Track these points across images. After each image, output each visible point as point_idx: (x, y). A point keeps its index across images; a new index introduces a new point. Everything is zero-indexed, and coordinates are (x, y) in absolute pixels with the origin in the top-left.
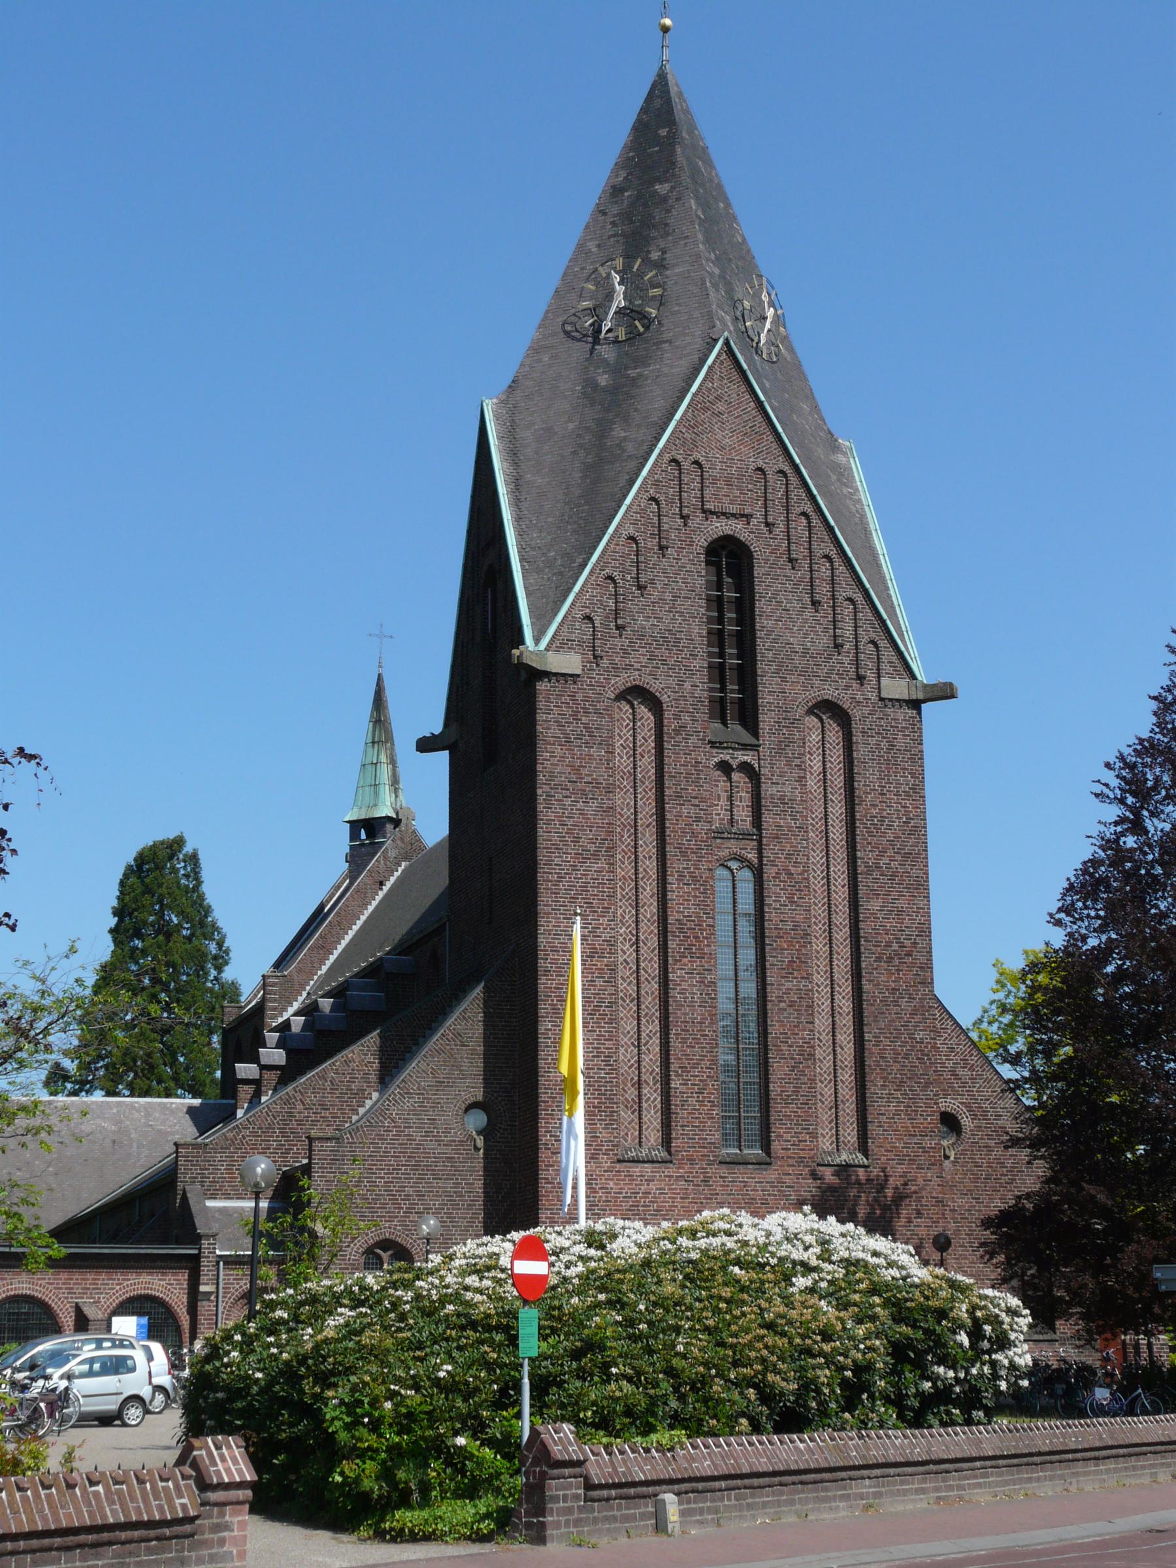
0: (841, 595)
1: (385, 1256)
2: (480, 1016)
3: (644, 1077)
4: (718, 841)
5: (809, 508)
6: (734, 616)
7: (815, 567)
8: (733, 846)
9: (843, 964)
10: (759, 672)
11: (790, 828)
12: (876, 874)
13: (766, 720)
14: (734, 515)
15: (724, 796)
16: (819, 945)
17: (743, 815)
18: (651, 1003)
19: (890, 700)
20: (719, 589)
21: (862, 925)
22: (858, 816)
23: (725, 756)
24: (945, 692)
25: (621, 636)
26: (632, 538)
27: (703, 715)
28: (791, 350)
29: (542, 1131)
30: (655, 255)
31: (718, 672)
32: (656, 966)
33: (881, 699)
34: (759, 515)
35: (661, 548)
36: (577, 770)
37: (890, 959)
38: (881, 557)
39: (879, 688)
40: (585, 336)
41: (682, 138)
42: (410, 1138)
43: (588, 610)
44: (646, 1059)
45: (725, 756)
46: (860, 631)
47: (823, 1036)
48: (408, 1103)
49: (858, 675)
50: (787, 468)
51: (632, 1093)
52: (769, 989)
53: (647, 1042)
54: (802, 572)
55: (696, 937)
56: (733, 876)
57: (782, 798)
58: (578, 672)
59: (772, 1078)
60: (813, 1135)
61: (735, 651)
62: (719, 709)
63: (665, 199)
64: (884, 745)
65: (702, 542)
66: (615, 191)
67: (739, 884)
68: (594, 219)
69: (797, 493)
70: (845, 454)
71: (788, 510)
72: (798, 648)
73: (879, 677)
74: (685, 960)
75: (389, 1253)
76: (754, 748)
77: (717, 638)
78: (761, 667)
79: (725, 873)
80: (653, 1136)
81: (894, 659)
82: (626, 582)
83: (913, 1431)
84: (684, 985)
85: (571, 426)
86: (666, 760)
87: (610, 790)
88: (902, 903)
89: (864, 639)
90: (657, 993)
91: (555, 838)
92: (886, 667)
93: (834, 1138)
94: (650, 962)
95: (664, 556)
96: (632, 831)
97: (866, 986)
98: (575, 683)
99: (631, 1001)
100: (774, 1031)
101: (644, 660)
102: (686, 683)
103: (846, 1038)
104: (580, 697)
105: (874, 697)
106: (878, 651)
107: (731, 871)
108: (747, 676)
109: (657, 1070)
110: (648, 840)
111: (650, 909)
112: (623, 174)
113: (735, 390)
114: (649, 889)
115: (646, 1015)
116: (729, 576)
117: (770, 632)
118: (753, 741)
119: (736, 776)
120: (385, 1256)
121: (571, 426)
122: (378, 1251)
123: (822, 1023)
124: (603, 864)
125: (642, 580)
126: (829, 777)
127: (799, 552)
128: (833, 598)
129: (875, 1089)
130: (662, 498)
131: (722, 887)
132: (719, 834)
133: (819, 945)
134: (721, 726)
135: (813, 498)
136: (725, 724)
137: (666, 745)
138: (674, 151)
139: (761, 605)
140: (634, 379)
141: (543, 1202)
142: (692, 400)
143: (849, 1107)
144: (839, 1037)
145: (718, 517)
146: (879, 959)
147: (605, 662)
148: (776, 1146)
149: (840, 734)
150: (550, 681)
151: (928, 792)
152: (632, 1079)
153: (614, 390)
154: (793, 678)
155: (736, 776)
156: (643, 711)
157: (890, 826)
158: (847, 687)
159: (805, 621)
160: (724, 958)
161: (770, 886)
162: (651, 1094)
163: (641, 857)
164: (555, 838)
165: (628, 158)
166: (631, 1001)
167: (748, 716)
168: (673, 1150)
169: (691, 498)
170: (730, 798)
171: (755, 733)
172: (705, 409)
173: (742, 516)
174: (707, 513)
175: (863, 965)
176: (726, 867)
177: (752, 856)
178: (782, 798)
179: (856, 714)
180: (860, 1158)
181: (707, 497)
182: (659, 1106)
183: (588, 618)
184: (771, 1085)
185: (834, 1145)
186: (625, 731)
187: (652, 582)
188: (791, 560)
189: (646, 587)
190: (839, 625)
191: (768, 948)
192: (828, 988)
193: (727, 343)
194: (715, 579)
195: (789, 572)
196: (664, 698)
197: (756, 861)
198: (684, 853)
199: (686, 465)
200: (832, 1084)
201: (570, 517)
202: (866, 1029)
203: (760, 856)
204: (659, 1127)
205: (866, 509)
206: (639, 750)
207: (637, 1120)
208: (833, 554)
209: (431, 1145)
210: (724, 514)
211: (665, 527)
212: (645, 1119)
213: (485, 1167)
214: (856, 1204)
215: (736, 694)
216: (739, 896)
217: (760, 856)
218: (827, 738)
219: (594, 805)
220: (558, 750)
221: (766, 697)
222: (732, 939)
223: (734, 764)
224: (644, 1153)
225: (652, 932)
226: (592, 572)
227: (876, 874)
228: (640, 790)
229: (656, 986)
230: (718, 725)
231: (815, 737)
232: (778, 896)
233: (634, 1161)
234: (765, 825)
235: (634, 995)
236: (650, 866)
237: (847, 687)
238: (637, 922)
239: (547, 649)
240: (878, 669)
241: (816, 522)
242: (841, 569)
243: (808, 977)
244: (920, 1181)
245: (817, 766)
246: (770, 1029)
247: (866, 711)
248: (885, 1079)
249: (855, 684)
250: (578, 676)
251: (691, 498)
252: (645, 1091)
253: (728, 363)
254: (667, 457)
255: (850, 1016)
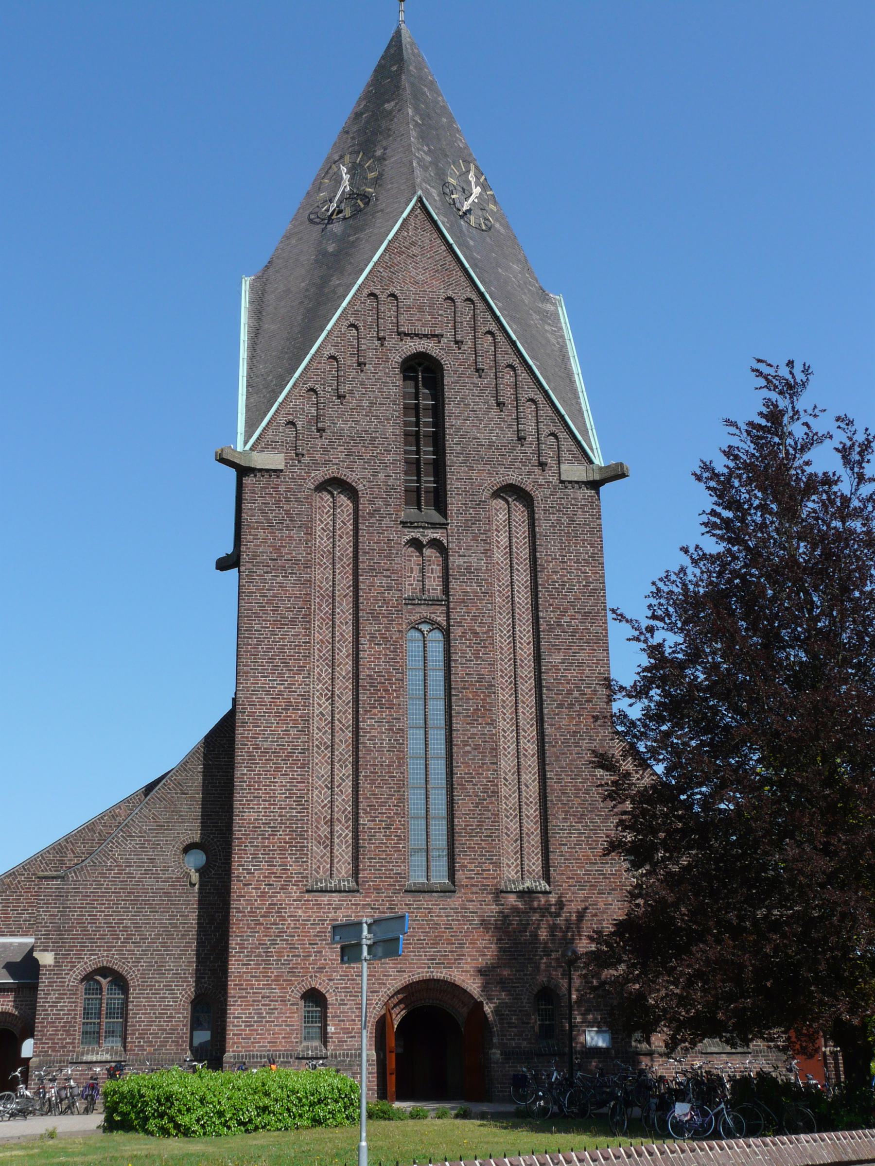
0: (524, 396)
1: (104, 982)
2: (200, 768)
3: (336, 816)
4: (409, 607)
5: (494, 328)
6: (431, 420)
7: (500, 375)
8: (424, 611)
9: (528, 712)
10: (448, 463)
11: (476, 594)
12: (558, 631)
13: (454, 503)
14: (425, 336)
15: (416, 569)
16: (504, 695)
17: (434, 586)
18: (344, 749)
19: (570, 482)
20: (417, 398)
21: (544, 676)
22: (540, 581)
23: (416, 534)
24: (617, 474)
25: (321, 437)
26: (333, 357)
27: (398, 498)
28: (507, 227)
29: (235, 865)
30: (379, 153)
31: (414, 466)
32: (350, 717)
33: (562, 482)
34: (449, 335)
35: (359, 364)
36: (277, 550)
37: (571, 706)
38: (576, 376)
39: (560, 473)
40: (323, 220)
41: (409, 71)
42: (130, 876)
43: (291, 417)
44: (339, 799)
45: (416, 534)
46: (541, 425)
47: (509, 776)
48: (130, 845)
49: (539, 462)
50: (474, 296)
51: (324, 830)
52: (454, 734)
53: (340, 785)
54: (488, 380)
55: (386, 690)
56: (424, 637)
57: (468, 569)
58: (281, 467)
59: (457, 813)
60: (497, 865)
61: (431, 449)
62: (414, 497)
63: (391, 112)
64: (565, 520)
65: (397, 358)
66: (357, 115)
67: (429, 645)
68: (340, 137)
69: (483, 315)
70: (554, 304)
71: (474, 330)
72: (485, 442)
73: (559, 463)
74: (376, 711)
75: (109, 979)
76: (443, 526)
77: (413, 438)
78: (450, 459)
79: (417, 634)
80: (344, 869)
81: (573, 448)
82: (327, 392)
83: (781, 1137)
84: (374, 733)
85: (303, 285)
86: (361, 539)
87: (307, 566)
88: (583, 656)
89: (545, 431)
90: (350, 741)
91: (256, 608)
92: (565, 455)
93: (519, 868)
94: (344, 713)
95: (362, 371)
96: (330, 601)
97: (548, 730)
98: (278, 477)
99: (326, 749)
100: (460, 771)
101: (342, 456)
102: (383, 472)
103: (530, 777)
104: (282, 488)
105: (555, 480)
106: (558, 442)
107: (422, 632)
108: (439, 468)
109: (349, 809)
110: (345, 607)
111: (346, 667)
112: (363, 103)
113: (428, 237)
114: (344, 651)
115: (340, 760)
116: (425, 386)
117: (458, 430)
118: (443, 521)
119: (427, 552)
120: (104, 982)
121: (303, 285)
122: (98, 978)
123: (507, 764)
124: (299, 629)
125: (341, 391)
126: (515, 550)
127: (486, 363)
128: (517, 399)
129: (557, 821)
130: (361, 324)
131: (412, 643)
132: (410, 601)
133: (504, 695)
134: (416, 511)
135: (497, 319)
136: (419, 509)
137: (361, 526)
138: (401, 78)
139: (450, 408)
140: (353, 242)
141: (234, 929)
142: (388, 245)
143: (535, 840)
144: (524, 777)
145: (412, 338)
146: (560, 706)
147: (306, 460)
148: (459, 875)
149: (526, 513)
150: (255, 476)
151: (606, 560)
152: (325, 817)
153: (336, 254)
154: (480, 467)
155: (427, 552)
156: (343, 499)
157: (570, 590)
158: (530, 473)
159: (491, 420)
160: (415, 709)
161: (457, 644)
162: (343, 831)
163: (338, 622)
164: (256, 608)
165: (369, 92)
166: (326, 749)
167: (440, 502)
168: (360, 880)
169: (388, 324)
170: (422, 571)
171: (445, 516)
172: (401, 253)
173: (434, 336)
174: (402, 335)
175: (545, 711)
176: (417, 629)
177: (441, 619)
178: (468, 569)
179: (538, 495)
180: (543, 885)
181: (401, 322)
182: (350, 841)
183: (291, 423)
184: (456, 820)
185: (519, 874)
186: (325, 516)
187: (351, 392)
188: (477, 370)
189: (344, 397)
190: (522, 421)
191: (454, 698)
192: (514, 733)
193: (420, 200)
194: (413, 391)
195: (476, 380)
196: (360, 487)
197: (445, 623)
198: (375, 618)
199: (382, 297)
200: (517, 819)
201: (289, 349)
202: (548, 768)
203: (448, 619)
204: (350, 860)
205: (568, 342)
206: (339, 532)
207: (328, 855)
208: (516, 363)
209: (149, 882)
210: (417, 335)
211: (363, 347)
212: (336, 853)
213: (199, 901)
214: (539, 928)
215: (429, 482)
216: (429, 655)
217: (448, 619)
218: (513, 517)
219: (292, 579)
220: (261, 534)
221: (453, 483)
222: (422, 692)
223: (425, 541)
224: (333, 884)
225: (347, 687)
226: (294, 385)
227: (558, 631)
228: (338, 566)
229: (350, 735)
230: (413, 511)
231: (502, 516)
232: (464, 652)
233: (322, 891)
234: (452, 592)
235: (329, 743)
236: (346, 630)
237: (530, 473)
238: (333, 679)
239: (251, 449)
240: (559, 457)
241: (500, 338)
242: (523, 375)
243: (493, 723)
244: (601, 906)
245: (504, 541)
246: (455, 770)
247: (548, 492)
248: (566, 813)
249: (537, 470)
250: (281, 471)
251: (388, 324)
252: (337, 828)
253: (422, 217)
254: (366, 292)
255: (535, 758)
